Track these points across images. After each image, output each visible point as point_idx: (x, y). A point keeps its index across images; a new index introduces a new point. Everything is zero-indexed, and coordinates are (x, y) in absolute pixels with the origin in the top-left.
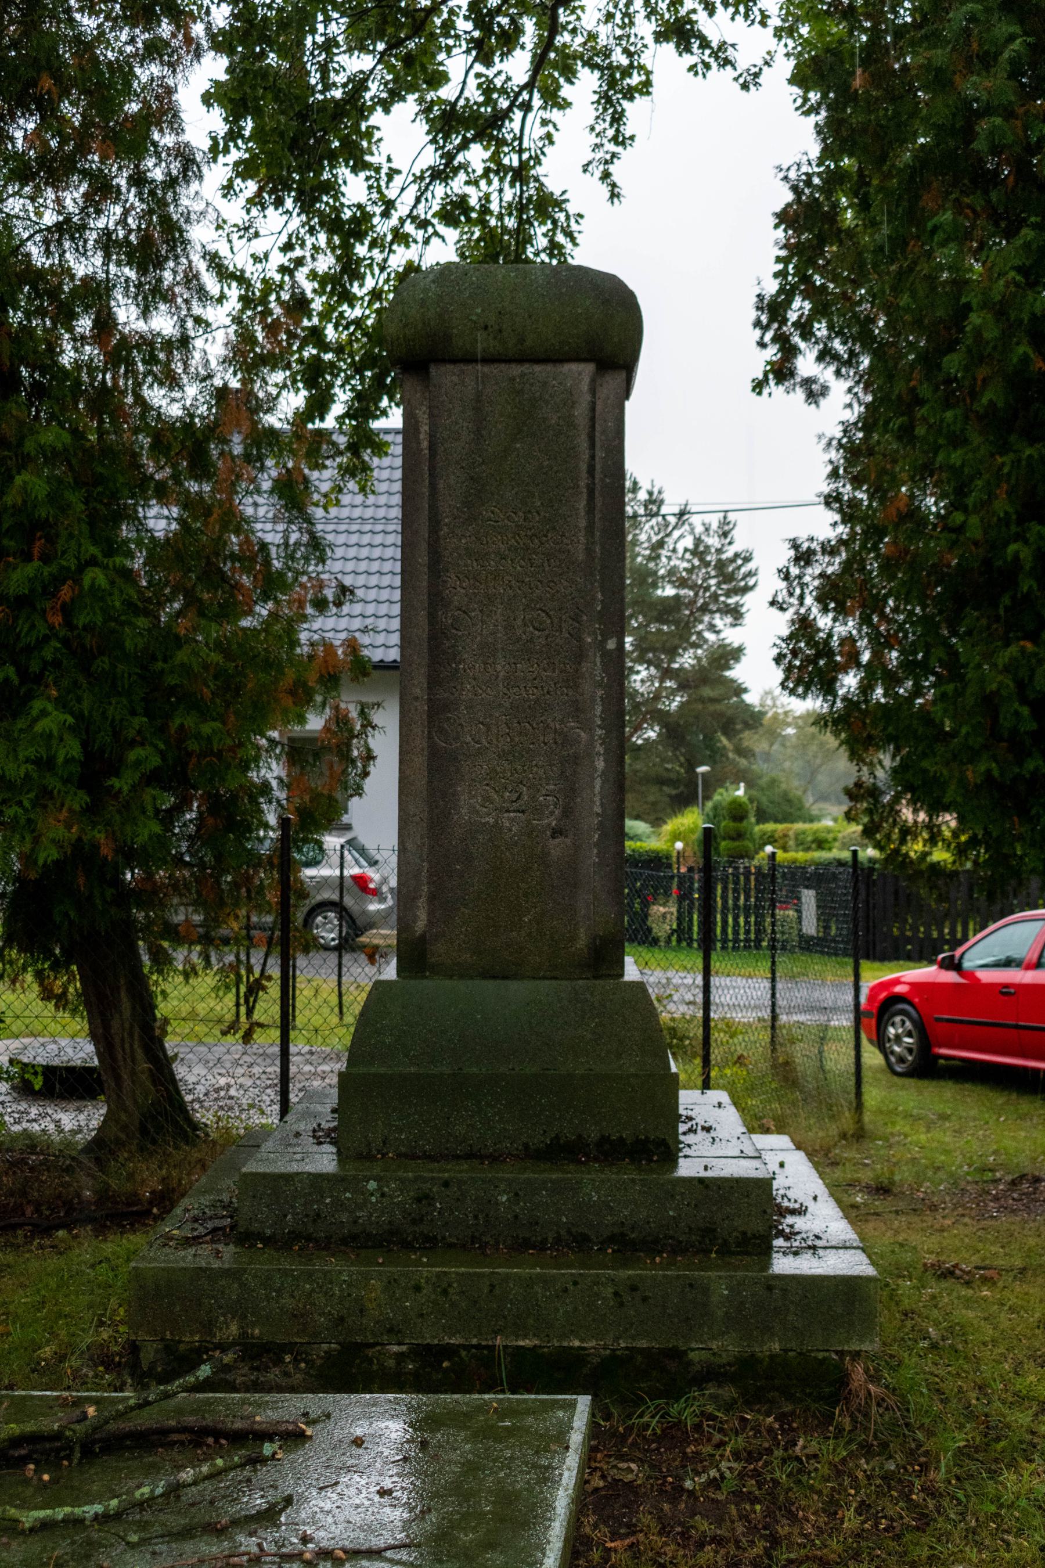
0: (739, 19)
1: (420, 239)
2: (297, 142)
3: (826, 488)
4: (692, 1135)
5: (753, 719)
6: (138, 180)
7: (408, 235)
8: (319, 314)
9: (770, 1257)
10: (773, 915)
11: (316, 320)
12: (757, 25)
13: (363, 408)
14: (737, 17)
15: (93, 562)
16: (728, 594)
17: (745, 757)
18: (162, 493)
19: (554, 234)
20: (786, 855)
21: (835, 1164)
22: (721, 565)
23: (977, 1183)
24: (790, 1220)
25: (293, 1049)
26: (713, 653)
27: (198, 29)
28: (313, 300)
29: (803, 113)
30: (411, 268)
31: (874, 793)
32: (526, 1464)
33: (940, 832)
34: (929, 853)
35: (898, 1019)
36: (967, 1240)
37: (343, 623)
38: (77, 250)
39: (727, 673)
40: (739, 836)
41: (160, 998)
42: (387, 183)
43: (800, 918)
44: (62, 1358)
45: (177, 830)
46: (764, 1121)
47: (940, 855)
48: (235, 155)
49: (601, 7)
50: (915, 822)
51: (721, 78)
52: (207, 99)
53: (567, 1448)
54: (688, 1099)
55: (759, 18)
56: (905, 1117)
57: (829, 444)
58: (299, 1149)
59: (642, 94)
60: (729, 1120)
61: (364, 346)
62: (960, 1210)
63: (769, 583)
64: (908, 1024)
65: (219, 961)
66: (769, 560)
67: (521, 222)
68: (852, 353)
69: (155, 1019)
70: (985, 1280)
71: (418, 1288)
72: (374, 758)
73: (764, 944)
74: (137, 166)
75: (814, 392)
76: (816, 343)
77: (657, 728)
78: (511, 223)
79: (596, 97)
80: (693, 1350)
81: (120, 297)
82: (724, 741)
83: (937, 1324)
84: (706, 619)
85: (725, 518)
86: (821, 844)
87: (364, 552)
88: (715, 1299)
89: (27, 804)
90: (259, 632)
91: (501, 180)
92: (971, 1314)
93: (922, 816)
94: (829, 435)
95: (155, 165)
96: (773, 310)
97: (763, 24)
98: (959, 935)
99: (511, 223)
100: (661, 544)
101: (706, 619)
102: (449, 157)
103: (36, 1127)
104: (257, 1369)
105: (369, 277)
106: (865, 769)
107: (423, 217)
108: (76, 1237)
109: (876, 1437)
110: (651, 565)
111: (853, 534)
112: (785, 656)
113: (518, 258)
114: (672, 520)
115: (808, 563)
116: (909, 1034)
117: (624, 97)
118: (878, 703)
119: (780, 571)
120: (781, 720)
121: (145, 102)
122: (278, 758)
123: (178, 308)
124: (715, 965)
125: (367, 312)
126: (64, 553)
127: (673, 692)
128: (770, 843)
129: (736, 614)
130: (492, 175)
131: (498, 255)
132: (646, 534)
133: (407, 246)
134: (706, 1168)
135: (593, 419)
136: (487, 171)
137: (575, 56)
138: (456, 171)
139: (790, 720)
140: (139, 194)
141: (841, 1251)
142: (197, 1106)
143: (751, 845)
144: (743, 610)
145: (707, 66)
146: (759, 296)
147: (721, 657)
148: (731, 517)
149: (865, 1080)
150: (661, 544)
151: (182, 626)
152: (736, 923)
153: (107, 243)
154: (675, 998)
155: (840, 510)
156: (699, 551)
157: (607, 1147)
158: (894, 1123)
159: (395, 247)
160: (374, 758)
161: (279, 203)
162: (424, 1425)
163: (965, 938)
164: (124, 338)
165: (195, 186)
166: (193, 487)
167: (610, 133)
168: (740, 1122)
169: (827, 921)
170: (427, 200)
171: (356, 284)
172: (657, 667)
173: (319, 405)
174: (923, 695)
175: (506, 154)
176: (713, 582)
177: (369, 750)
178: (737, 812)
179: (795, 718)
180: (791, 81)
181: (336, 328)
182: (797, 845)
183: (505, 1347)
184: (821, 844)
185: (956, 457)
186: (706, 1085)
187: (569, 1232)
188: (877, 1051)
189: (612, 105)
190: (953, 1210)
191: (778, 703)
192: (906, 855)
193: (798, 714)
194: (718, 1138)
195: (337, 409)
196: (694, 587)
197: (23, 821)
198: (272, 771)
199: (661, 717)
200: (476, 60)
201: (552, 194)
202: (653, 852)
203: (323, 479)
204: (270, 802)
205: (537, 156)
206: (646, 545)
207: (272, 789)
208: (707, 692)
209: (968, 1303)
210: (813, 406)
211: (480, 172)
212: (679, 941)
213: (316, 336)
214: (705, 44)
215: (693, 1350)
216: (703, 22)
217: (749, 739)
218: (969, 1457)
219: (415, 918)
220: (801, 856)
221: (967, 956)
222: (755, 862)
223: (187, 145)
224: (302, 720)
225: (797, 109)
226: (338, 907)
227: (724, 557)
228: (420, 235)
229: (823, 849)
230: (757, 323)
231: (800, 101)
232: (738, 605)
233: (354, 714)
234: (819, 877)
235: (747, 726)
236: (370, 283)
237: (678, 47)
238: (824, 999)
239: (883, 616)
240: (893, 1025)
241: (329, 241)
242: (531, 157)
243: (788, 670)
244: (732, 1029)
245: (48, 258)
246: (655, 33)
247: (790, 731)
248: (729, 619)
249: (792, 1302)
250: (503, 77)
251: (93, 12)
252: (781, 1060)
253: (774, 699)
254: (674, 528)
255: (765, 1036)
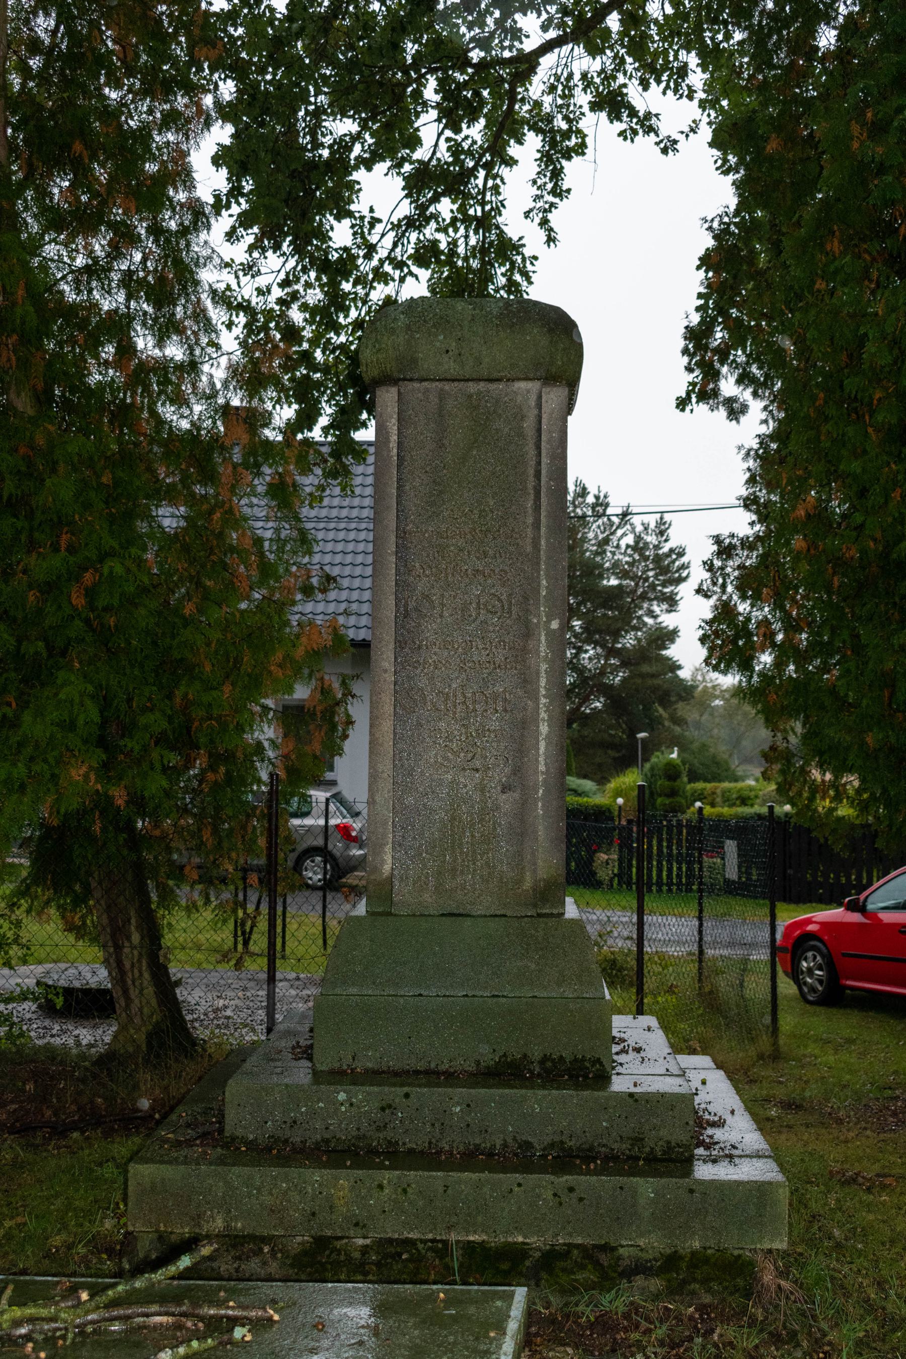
0: (670, 93)
1: (397, 277)
2: (290, 194)
3: (744, 492)
4: (624, 1055)
5: (686, 691)
6: (156, 230)
7: (387, 274)
8: (309, 341)
9: (692, 1165)
10: (700, 863)
11: (305, 346)
12: (685, 99)
13: (345, 421)
14: (668, 92)
15: (111, 554)
16: (664, 585)
17: (679, 725)
18: (170, 495)
19: (512, 274)
20: (713, 810)
21: (752, 1081)
22: (658, 559)
23: (877, 1099)
24: (710, 1131)
25: (279, 975)
26: (651, 635)
27: (208, 100)
28: (304, 328)
29: (722, 173)
30: (389, 302)
31: (787, 757)
32: (467, 1348)
33: (845, 790)
34: (836, 809)
35: (810, 954)
36: (868, 1150)
37: (321, 607)
38: (103, 288)
39: (664, 652)
40: (673, 793)
41: (166, 930)
42: (370, 230)
43: (724, 865)
44: (70, 1247)
45: (182, 784)
46: (691, 1043)
47: (844, 811)
48: (235, 209)
49: (545, 80)
50: (823, 781)
51: (646, 142)
52: (216, 161)
53: (505, 1334)
54: (620, 1023)
55: (686, 93)
56: (815, 1041)
57: (748, 454)
58: (279, 1064)
59: (578, 154)
60: (656, 1042)
61: (347, 367)
62: (863, 1124)
63: (698, 575)
64: (818, 958)
65: (217, 898)
66: (698, 552)
67: (483, 263)
68: (767, 376)
69: (160, 948)
70: (884, 1187)
71: (381, 1187)
72: (352, 723)
73: (695, 887)
74: (155, 218)
75: (735, 410)
76: (736, 368)
77: (602, 700)
78: (475, 264)
79: (539, 155)
80: (622, 1246)
81: (139, 328)
82: (661, 710)
83: (841, 1226)
84: (645, 605)
85: (661, 518)
86: (744, 801)
87: (351, 547)
88: (642, 1201)
89: (51, 761)
90: (255, 613)
91: (466, 229)
92: (871, 1217)
93: (828, 776)
94: (747, 446)
95: (170, 218)
96: (696, 337)
97: (690, 97)
98: (864, 881)
99: (475, 264)
100: (606, 541)
101: (645, 605)
102: (422, 208)
103: (57, 1041)
104: (238, 1258)
105: (353, 309)
106: (779, 734)
107: (399, 258)
108: (88, 1138)
109: (785, 1327)
110: (598, 559)
111: (768, 532)
112: (709, 636)
113: (483, 294)
114: (616, 520)
115: (730, 556)
116: (820, 969)
117: (563, 157)
118: (790, 676)
119: (704, 563)
120: (712, 692)
121: (163, 163)
122: (269, 722)
123: (188, 338)
124: (648, 903)
125: (351, 339)
126: (86, 545)
127: (615, 670)
128: (700, 800)
129: (672, 602)
130: (458, 224)
131: (464, 291)
132: (594, 532)
133: (386, 284)
134: (635, 1085)
135: (539, 430)
136: (454, 220)
137: (524, 121)
138: (427, 220)
139: (717, 693)
140: (156, 241)
141: (755, 1160)
142: (197, 1025)
143: (683, 801)
144: (678, 598)
145: (635, 132)
146: (686, 327)
147: (658, 638)
148: (667, 517)
149: (780, 1007)
150: (606, 541)
151: (189, 609)
152: (670, 870)
153: (128, 279)
154: (616, 934)
155: (757, 512)
156: (639, 546)
157: (549, 1064)
158: (806, 1046)
159: (375, 284)
160: (352, 723)
161: (277, 247)
162: (382, 1309)
163: (870, 884)
164: (141, 363)
165: (203, 236)
166: (198, 489)
167: (549, 186)
168: (667, 1044)
169: (749, 868)
170: (403, 244)
171: (342, 316)
172: (603, 646)
173: (306, 419)
174: (828, 672)
175: (471, 206)
176: (651, 574)
177: (348, 716)
178: (671, 772)
179: (722, 691)
180: (711, 145)
181: (324, 353)
182: (724, 802)
183: (458, 1242)
184: (744, 801)
185: (855, 466)
186: (640, 1011)
187: (515, 1139)
188: (792, 983)
189: (553, 163)
190: (856, 1124)
191: (707, 678)
192: (816, 810)
193: (725, 687)
194: (648, 1060)
195: (323, 421)
196: (634, 578)
197: (48, 776)
198: (267, 733)
199: (606, 690)
200: (445, 127)
201: (511, 239)
202: (597, 806)
203: (309, 482)
204: (263, 761)
205: (498, 208)
206: (593, 542)
207: (264, 749)
208: (646, 668)
209: (869, 1207)
210: (734, 422)
211: (448, 221)
212: (619, 884)
213: (307, 357)
214: (633, 113)
215: (622, 1246)
216: (634, 94)
217: (682, 709)
218: (868, 1346)
219: (383, 862)
220: (726, 811)
221: (870, 900)
222: (688, 815)
223: (198, 200)
224: (290, 689)
225: (717, 169)
226: (323, 851)
227: (661, 552)
228: (397, 274)
229: (746, 805)
230: (685, 351)
231: (720, 162)
232: (673, 595)
233: (336, 685)
234: (741, 830)
235: (681, 698)
236: (353, 314)
237: (609, 116)
238: (745, 936)
239: (794, 601)
240: (806, 959)
241: (318, 279)
242: (492, 209)
243: (711, 650)
244: (664, 960)
245: (78, 294)
246: (590, 102)
247: (718, 702)
248: (665, 606)
249: (710, 1205)
250: (469, 141)
251: (118, 86)
252: (707, 990)
253: (703, 676)
254: (617, 528)
255: (693, 968)
